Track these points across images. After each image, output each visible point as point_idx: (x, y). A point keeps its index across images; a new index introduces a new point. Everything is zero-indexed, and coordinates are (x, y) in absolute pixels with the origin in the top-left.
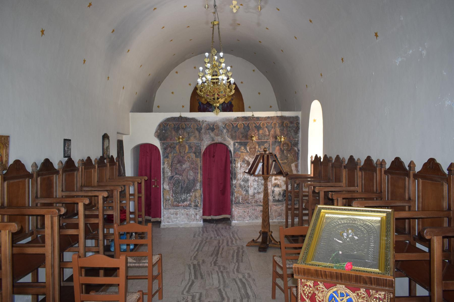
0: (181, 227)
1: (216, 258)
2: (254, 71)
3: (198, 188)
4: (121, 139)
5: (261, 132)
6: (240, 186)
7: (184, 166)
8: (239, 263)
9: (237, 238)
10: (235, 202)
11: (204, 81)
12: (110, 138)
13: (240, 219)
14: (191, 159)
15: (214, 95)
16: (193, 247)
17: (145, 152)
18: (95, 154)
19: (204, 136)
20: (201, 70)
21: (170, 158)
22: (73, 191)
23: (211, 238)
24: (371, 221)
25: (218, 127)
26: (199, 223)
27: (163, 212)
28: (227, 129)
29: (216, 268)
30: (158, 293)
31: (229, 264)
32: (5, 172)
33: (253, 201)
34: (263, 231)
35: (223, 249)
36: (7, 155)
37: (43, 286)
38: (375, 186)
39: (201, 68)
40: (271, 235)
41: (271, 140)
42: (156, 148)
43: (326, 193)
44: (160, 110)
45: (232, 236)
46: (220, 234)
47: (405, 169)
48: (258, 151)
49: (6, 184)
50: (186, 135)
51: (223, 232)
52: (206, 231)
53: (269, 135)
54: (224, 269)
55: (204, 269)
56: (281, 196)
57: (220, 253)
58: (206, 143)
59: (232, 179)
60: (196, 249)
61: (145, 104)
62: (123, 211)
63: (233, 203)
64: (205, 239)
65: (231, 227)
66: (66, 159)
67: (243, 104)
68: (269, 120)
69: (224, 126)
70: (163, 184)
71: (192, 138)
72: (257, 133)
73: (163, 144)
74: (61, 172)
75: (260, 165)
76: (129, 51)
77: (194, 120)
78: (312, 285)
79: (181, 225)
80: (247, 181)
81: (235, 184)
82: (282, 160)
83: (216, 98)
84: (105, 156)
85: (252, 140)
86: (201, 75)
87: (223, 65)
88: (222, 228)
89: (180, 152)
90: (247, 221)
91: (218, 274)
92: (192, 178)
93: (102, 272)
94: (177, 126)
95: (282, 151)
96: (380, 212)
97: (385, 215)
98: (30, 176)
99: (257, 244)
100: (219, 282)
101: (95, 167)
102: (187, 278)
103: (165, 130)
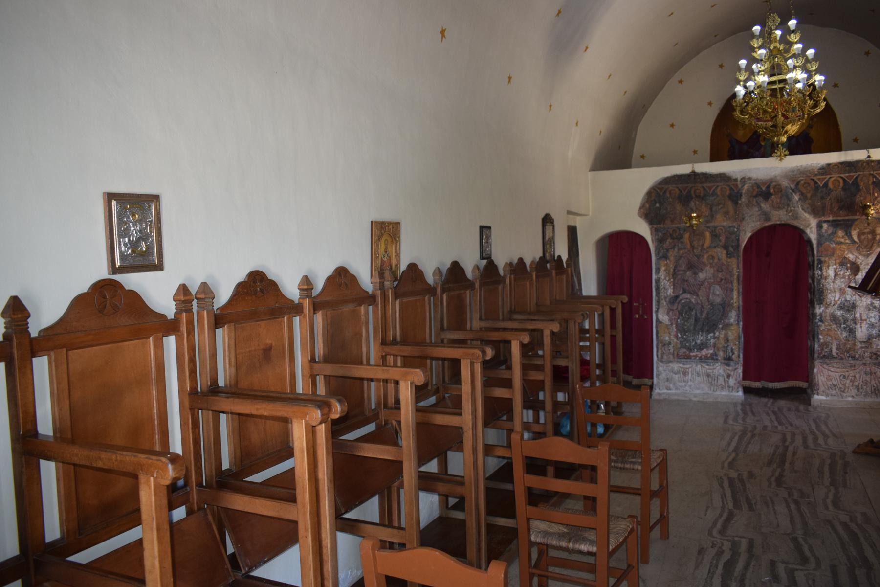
1: (779, 470)
2: (867, 53)
3: (732, 321)
6: (834, 318)
7: (702, 276)
9: (827, 432)
10: (820, 354)
12: (555, 223)
13: (834, 392)
14: (716, 261)
17: (620, 248)
18: (531, 253)
20: (743, 67)
21: (672, 258)
22: (497, 319)
25: (779, 189)
26: (734, 394)
27: (657, 368)
28: (802, 194)
32: (396, 283)
33: (867, 354)
35: (795, 453)
36: (398, 255)
37: (459, 481)
39: (743, 62)
44: (645, 161)
45: (814, 427)
49: (397, 302)
50: (705, 210)
52: (752, 412)
57: (788, 461)
60: (731, 448)
61: (616, 154)
63: (816, 355)
65: (810, 409)
66: (485, 262)
69: (793, 186)
71: (719, 217)
73: (657, 230)
74: (477, 285)
76: (587, 48)
77: (723, 177)
80: (851, 307)
81: (821, 315)
84: (548, 257)
85: (867, 215)
86: (742, 78)
88: (789, 410)
89: (693, 247)
90: (850, 399)
91: (788, 507)
92: (718, 300)
93: (550, 470)
98: (431, 290)
100: (792, 522)
101: (532, 276)
103: (660, 203)
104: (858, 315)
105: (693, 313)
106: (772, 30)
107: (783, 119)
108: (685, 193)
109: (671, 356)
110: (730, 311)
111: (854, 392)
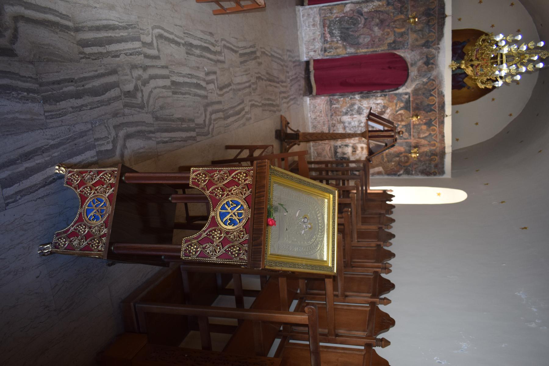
1: (265, 78)
2: (511, 115)
5: (424, 127)
7: (376, 29)
8: (261, 106)
9: (290, 104)
11: (499, 44)
13: (312, 107)
14: (386, 37)
15: (478, 59)
21: (387, 9)
24: (322, 250)
25: (430, 70)
26: (305, 55)
27: (316, 7)
28: (427, 83)
29: (253, 80)
30: (219, 8)
31: (259, 95)
33: (334, 122)
34: (300, 134)
35: (276, 87)
38: (360, 260)
39: (519, 37)
40: (295, 144)
41: (413, 141)
43: (349, 205)
45: (292, 97)
46: (293, 82)
47: (381, 293)
48: (398, 125)
52: (295, 66)
53: (419, 138)
55: (252, 64)
56: (342, 156)
57: (271, 83)
58: (408, 56)
59: (361, 93)
60: (273, 53)
63: (331, 97)
65: (301, 96)
68: (440, 137)
69: (432, 78)
72: (421, 122)
75: (381, 127)
77: (441, 35)
78: (247, 182)
79: (301, 33)
80: (359, 112)
81: (355, 98)
82: (386, 155)
83: (472, 63)
85: (412, 117)
86: (508, 38)
87: (524, 69)
88: (300, 85)
90: (309, 115)
91: (247, 82)
92: (361, 40)
95: (398, 155)
96: (333, 260)
97: (330, 265)
99: (284, 128)
100: (239, 84)
102: (241, 44)
104: (355, 116)
105: (352, 26)
106: (538, 54)
107: (476, 65)
108: (432, 12)
109: (324, 15)
110: (354, 49)
111: (313, 117)
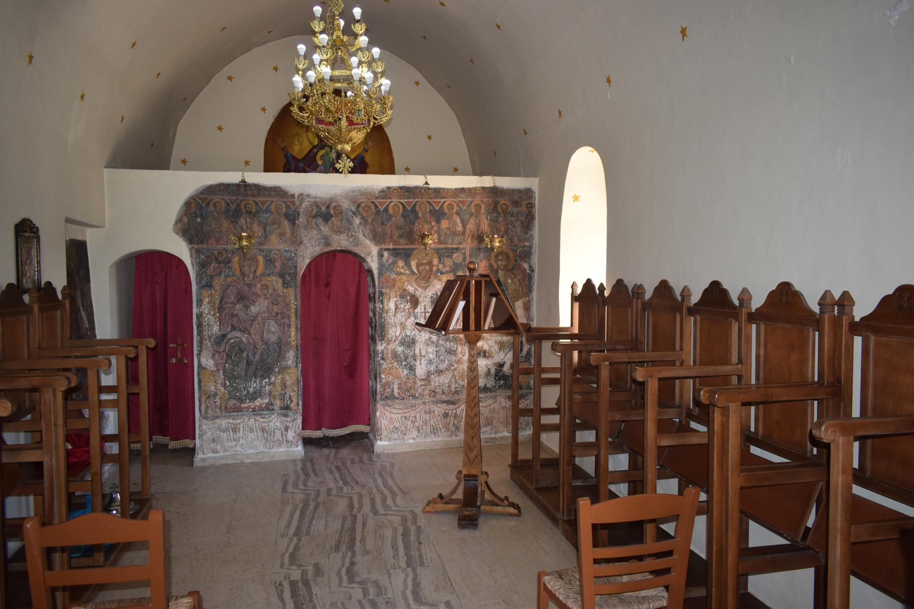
0: (248, 461)
2: (417, 83)
3: (290, 362)
4: (79, 238)
5: (444, 224)
6: (395, 355)
7: (254, 309)
8: (414, 570)
9: (395, 488)
10: (382, 395)
13: (396, 436)
14: (271, 291)
16: (284, 523)
17: (149, 272)
19: (303, 233)
23: (329, 490)
25: (339, 211)
26: (294, 449)
27: (200, 426)
28: (363, 218)
34: (465, 472)
35: (364, 524)
39: (302, 48)
41: (468, 245)
42: (180, 262)
45: (380, 483)
50: (258, 230)
51: (356, 470)
52: (314, 470)
53: (464, 233)
54: (379, 594)
57: (358, 537)
59: (373, 339)
62: (79, 440)
63: (378, 397)
64: (313, 496)
67: (392, 160)
69: (353, 209)
70: (199, 355)
71: (274, 238)
72: (435, 228)
73: (198, 251)
77: (277, 191)
79: (248, 457)
81: (383, 352)
85: (425, 245)
86: (301, 67)
87: (363, 40)
89: (243, 274)
90: (411, 441)
92: (273, 338)
94: (233, 207)
103: (202, 216)
